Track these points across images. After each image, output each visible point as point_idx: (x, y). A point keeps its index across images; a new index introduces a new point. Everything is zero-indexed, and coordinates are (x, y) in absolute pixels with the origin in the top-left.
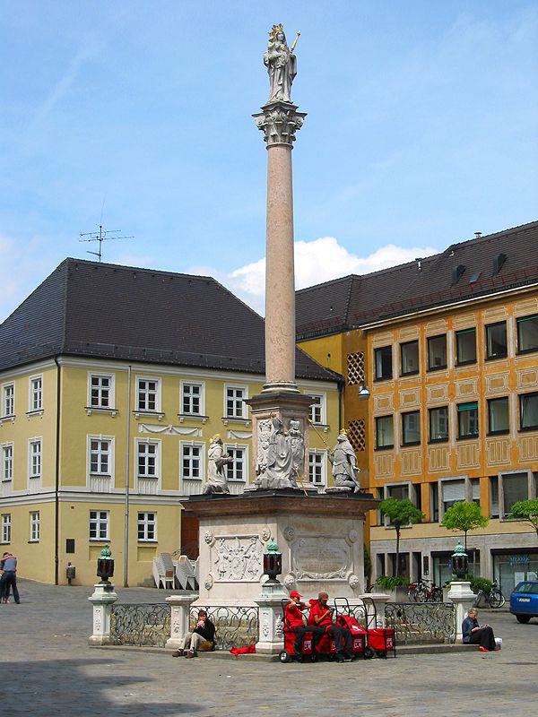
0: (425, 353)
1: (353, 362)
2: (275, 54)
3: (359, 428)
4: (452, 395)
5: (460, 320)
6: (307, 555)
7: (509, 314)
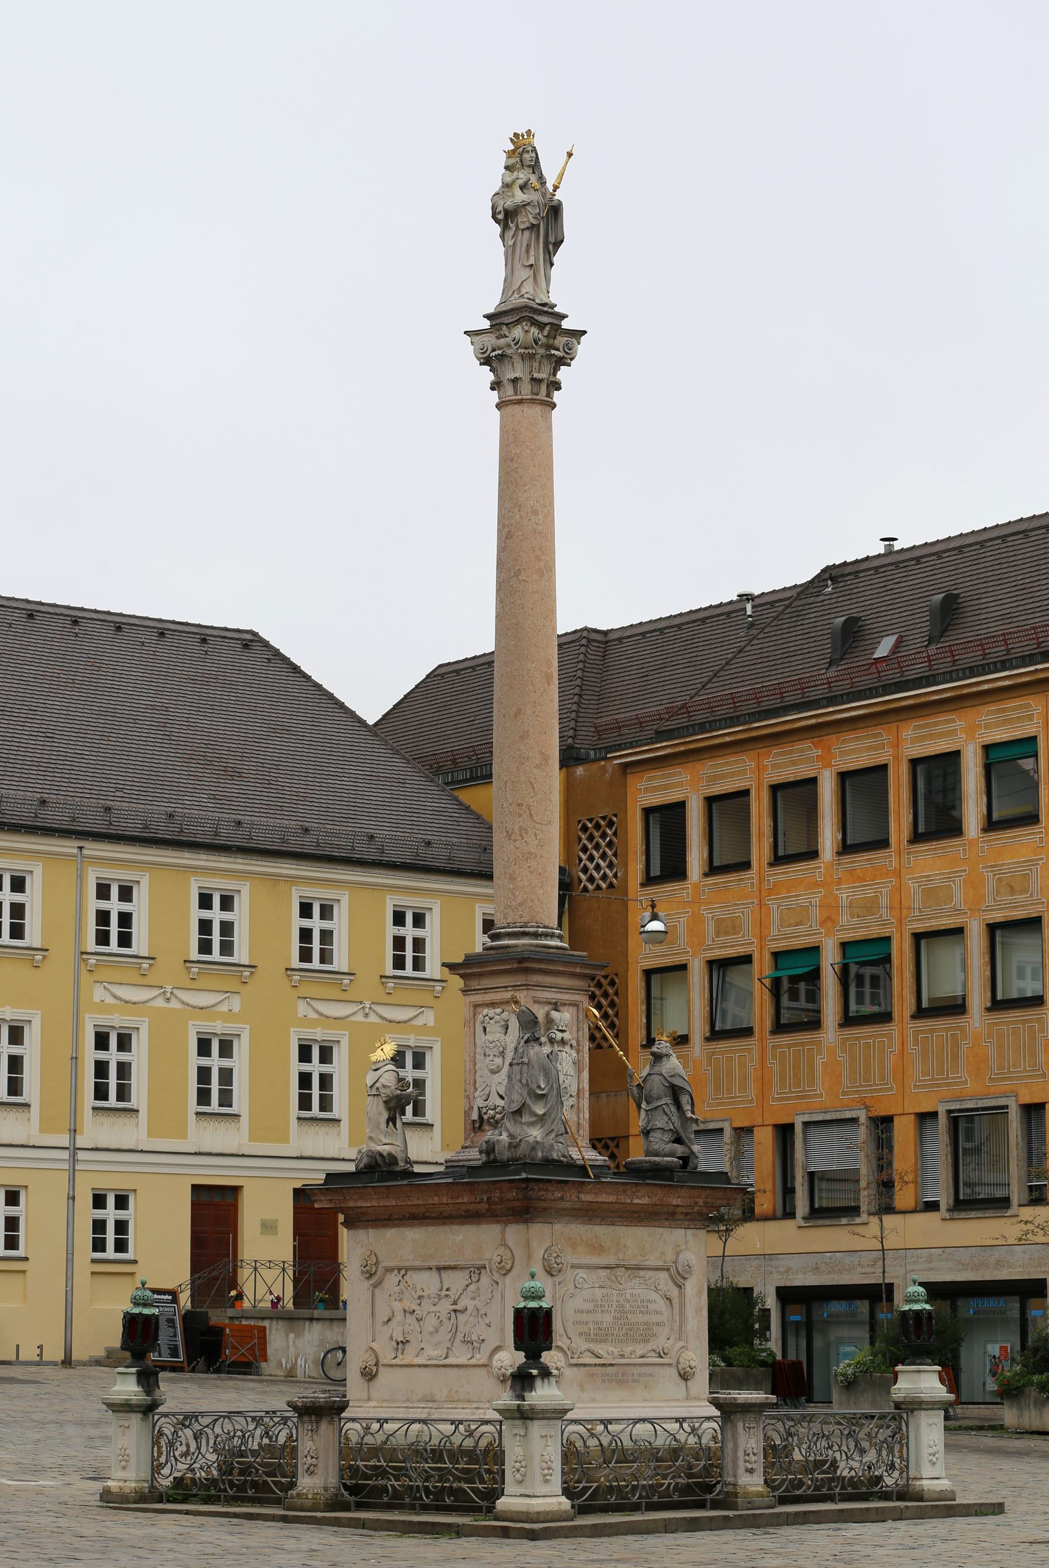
0: (767, 823)
1: (591, 838)
2: (520, 197)
4: (829, 920)
5: (852, 746)
7: (967, 737)
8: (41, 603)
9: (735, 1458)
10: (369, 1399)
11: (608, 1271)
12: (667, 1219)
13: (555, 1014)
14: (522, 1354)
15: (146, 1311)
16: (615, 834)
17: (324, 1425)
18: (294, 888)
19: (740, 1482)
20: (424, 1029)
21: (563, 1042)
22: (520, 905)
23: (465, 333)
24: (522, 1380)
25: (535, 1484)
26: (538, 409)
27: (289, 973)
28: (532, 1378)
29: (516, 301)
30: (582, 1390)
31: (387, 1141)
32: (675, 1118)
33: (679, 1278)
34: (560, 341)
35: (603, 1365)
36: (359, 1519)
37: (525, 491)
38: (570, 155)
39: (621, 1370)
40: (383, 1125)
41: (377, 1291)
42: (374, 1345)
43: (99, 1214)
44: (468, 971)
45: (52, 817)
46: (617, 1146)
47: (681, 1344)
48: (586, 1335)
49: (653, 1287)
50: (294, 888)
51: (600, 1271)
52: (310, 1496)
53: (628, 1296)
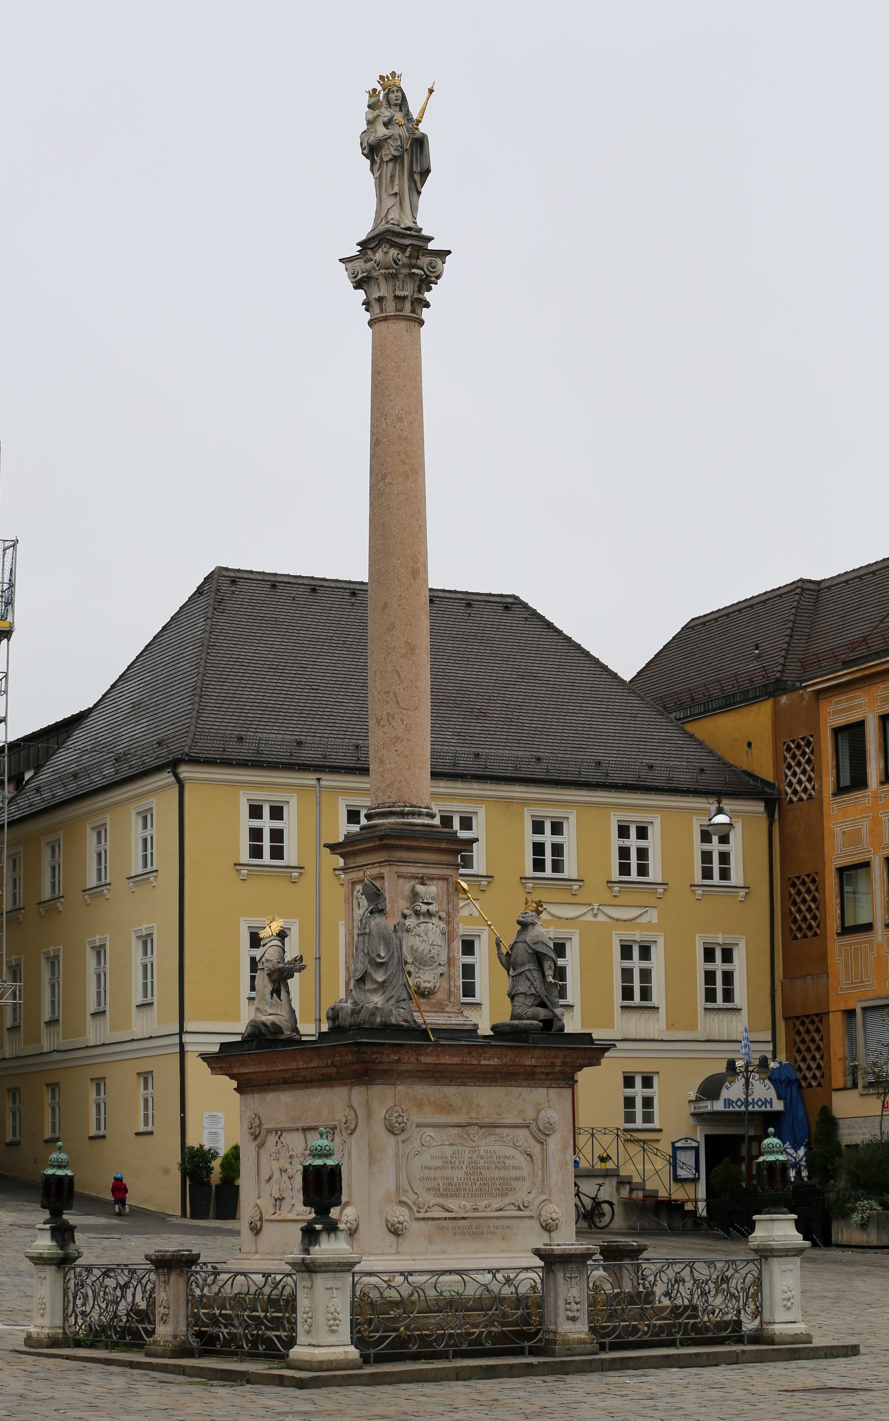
1: (794, 757)
2: (381, 131)
3: (809, 891)
6: (439, 1163)
8: (325, 580)
9: (556, 1307)
10: (256, 1252)
11: (460, 1129)
12: (525, 1079)
13: (420, 888)
14: (47, 1211)
15: (60, 1172)
16: (812, 752)
17: (173, 1277)
18: (526, 809)
19: (560, 1330)
20: (649, 926)
21: (429, 914)
22: (389, 786)
23: (340, 260)
24: (310, 1235)
25: (325, 1334)
26: (402, 324)
27: (523, 881)
28: (318, 1232)
29: (383, 227)
30: (431, 1242)
31: (272, 1012)
32: (538, 983)
33: (542, 1134)
34: (424, 261)
35: (454, 1218)
36: (180, 1366)
37: (391, 401)
38: (431, 91)
39: (475, 1223)
40: (268, 997)
41: (262, 1151)
42: (259, 1202)
43: (629, 1092)
44: (344, 850)
45: (306, 755)
46: (821, 1021)
47: (544, 1197)
48: (435, 1191)
49: (511, 1144)
50: (526, 809)
51: (451, 1129)
52: (162, 1344)
53: (482, 1153)
